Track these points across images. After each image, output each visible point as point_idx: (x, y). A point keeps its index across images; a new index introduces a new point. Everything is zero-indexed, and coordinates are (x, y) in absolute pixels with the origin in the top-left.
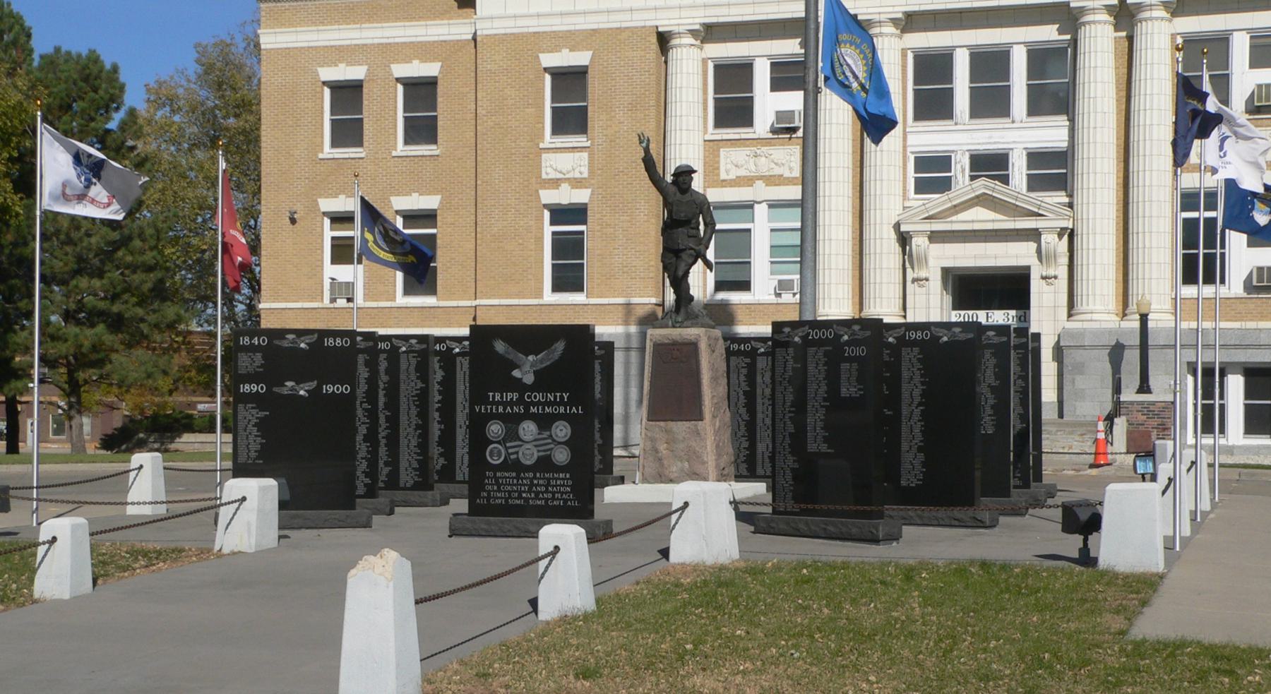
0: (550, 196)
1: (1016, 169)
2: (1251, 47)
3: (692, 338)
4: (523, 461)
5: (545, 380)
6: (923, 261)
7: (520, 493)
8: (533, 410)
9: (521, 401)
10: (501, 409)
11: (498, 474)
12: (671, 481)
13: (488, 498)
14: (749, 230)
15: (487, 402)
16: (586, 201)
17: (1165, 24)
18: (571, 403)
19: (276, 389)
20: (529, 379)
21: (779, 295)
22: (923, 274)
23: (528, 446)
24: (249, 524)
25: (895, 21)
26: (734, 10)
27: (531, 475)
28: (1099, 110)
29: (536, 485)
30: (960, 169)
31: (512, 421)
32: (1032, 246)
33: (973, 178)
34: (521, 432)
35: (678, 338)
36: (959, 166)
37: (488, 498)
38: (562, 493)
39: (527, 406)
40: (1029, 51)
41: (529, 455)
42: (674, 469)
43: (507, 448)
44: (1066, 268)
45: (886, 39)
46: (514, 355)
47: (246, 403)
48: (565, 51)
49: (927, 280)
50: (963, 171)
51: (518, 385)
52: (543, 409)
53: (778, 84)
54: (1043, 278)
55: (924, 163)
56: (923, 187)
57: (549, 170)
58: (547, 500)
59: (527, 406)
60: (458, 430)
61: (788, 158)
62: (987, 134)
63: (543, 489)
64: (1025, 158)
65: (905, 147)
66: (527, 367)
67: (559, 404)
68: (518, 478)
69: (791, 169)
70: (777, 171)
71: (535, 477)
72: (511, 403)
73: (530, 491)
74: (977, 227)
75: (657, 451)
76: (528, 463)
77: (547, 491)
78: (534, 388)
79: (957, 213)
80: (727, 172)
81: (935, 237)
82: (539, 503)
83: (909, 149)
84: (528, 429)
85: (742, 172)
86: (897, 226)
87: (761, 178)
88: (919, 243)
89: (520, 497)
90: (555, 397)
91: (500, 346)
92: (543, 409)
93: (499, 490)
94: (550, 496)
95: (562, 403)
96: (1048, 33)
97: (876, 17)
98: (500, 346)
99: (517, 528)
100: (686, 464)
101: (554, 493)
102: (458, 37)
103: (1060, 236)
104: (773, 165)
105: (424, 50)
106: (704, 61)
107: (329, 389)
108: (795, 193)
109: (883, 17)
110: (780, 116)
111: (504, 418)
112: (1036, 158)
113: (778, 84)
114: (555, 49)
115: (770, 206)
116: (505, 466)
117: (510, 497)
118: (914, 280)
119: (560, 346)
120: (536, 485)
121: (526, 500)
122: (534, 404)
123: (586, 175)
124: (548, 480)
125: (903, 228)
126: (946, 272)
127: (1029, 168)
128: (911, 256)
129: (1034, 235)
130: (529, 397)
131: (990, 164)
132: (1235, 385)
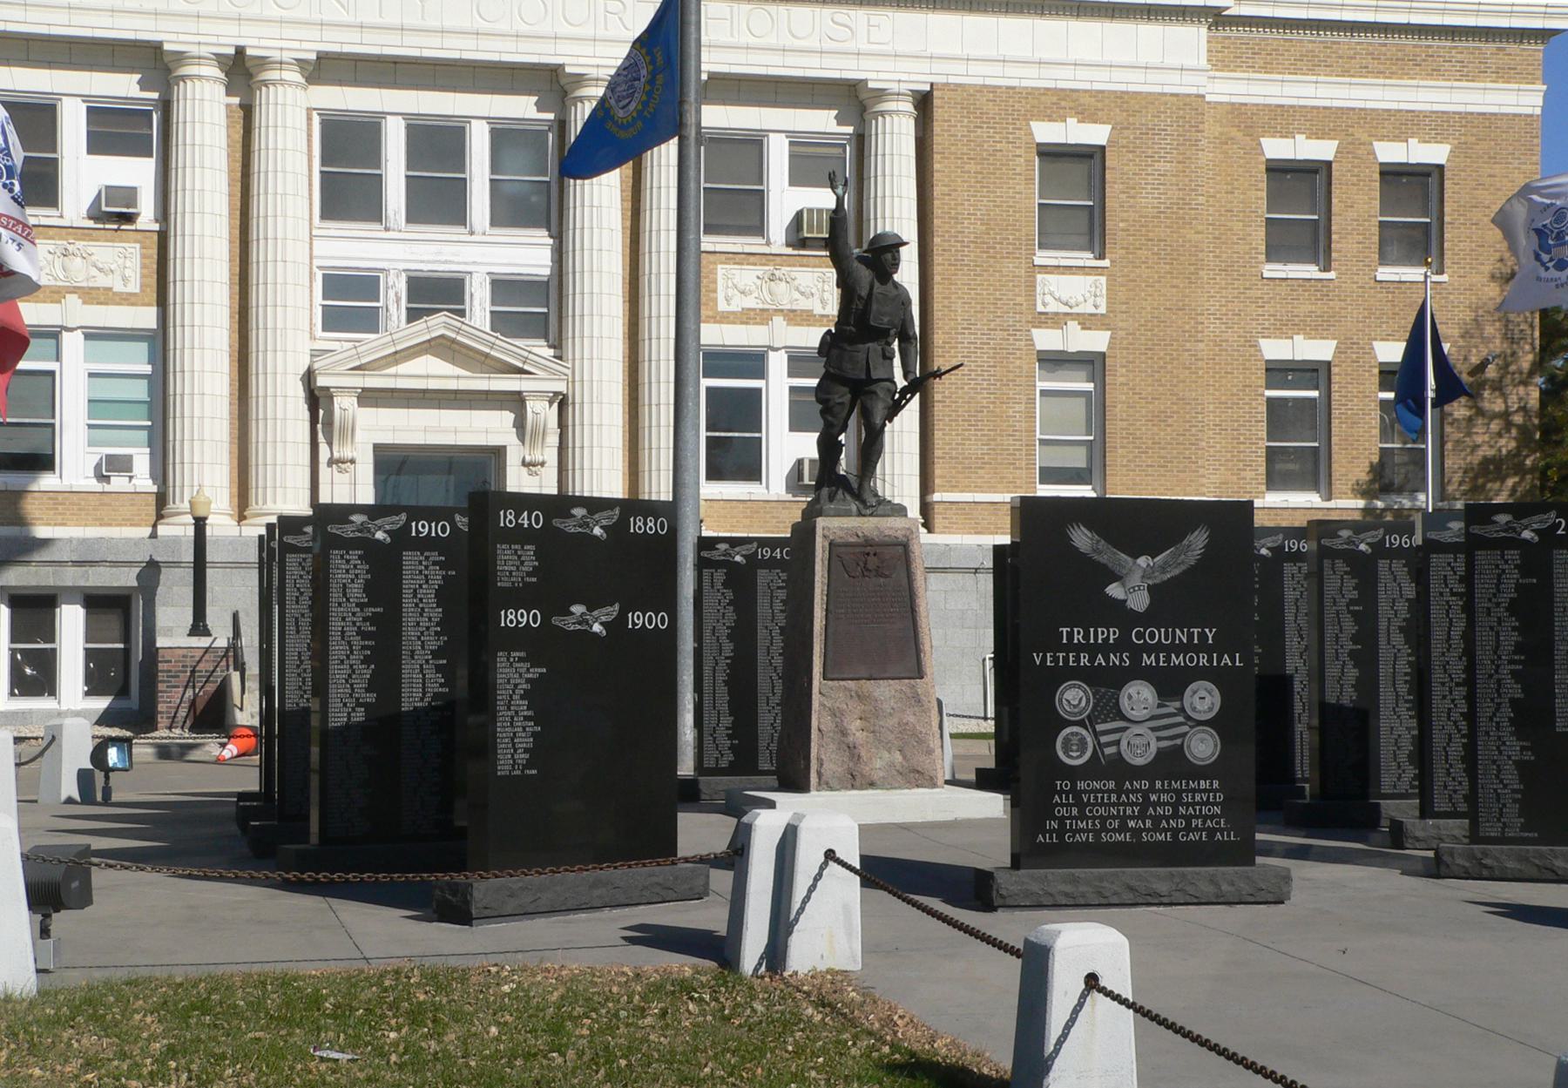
0: (1047, 340)
1: (476, 302)
2: (791, 156)
3: (899, 534)
4: (1128, 756)
5: (1170, 602)
6: (349, 432)
7: (1123, 820)
8: (1147, 660)
9: (1123, 644)
10: (1084, 660)
11: (1081, 785)
12: (872, 785)
13: (1061, 831)
14: (52, 373)
15: (1057, 646)
16: (1103, 348)
17: (299, 92)
18: (1220, 647)
19: (556, 621)
20: (1139, 601)
21: (106, 479)
22: (347, 453)
23: (1137, 729)
24: (846, 908)
25: (301, 63)
26: (78, 19)
27: (1145, 784)
28: (605, 225)
29: (1155, 805)
30: (394, 298)
31: (1106, 683)
32: (508, 417)
33: (413, 315)
34: (1125, 703)
35: (875, 535)
36: (391, 294)
37: (1061, 831)
38: (1205, 818)
39: (1136, 653)
40: (408, 127)
41: (1140, 747)
42: (879, 762)
43: (1096, 734)
44: (555, 451)
45: (289, 90)
46: (1110, 556)
47: (509, 649)
48: (1072, 121)
49: (352, 461)
50: (398, 301)
51: (1118, 613)
52: (1168, 659)
53: (99, 143)
54: (524, 464)
55: (337, 284)
56: (334, 320)
57: (1048, 298)
58: (1175, 832)
59: (1136, 653)
60: (762, 707)
61: (121, 262)
62: (434, 248)
63: (1169, 811)
64: (488, 287)
65: (311, 258)
66: (1135, 580)
67: (1197, 649)
68: (1119, 791)
69: (125, 279)
70: (102, 281)
71: (1152, 789)
72: (1105, 648)
73: (1142, 816)
74: (433, 385)
75: (844, 733)
76: (1139, 761)
77: (1175, 815)
78: (1146, 619)
79: (397, 363)
80: (1044, 304)
81: (369, 397)
82: (1161, 837)
83: (316, 262)
84: (1139, 697)
85: (751, 303)
86: (309, 377)
87: (74, 290)
88: (344, 405)
89: (1123, 828)
90: (1191, 636)
91: (1082, 538)
92: (1168, 659)
93: (1082, 817)
94: (1182, 823)
95: (1203, 647)
96: (123, 86)
97: (276, 55)
98: (1082, 538)
99: (1131, 889)
100: (898, 757)
101: (1188, 819)
102: (1327, 103)
103: (551, 403)
104: (94, 272)
105: (1319, 121)
106: (309, 110)
107: (637, 619)
108: (146, 317)
109: (287, 56)
110: (113, 193)
111: (1091, 677)
112: (503, 287)
113: (99, 143)
114: (1400, 136)
115: (88, 337)
116: (1094, 769)
117: (1104, 829)
118: (331, 462)
119: (1198, 540)
120: (1155, 805)
121: (1136, 832)
122: (1150, 650)
123: (1103, 310)
124: (1179, 792)
125: (321, 381)
126: (377, 448)
127: (493, 303)
128: (329, 424)
129: (515, 402)
130: (1140, 636)
131: (435, 293)
132: (71, 621)
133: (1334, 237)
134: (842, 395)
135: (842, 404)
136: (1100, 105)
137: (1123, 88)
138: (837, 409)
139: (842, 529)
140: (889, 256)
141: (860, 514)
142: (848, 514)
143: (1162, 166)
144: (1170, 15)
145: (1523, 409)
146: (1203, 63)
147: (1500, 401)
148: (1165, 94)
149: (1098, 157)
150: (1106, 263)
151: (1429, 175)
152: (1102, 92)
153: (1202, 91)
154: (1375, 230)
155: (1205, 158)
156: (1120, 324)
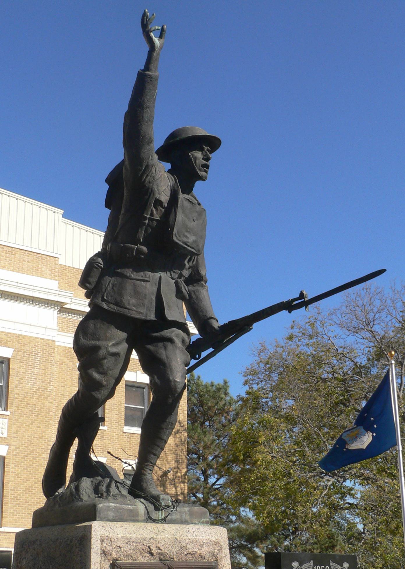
3: (205, 551)
35: (172, 551)
123: (5, 435)
133: (106, 411)
134: (115, 340)
135: (116, 355)
136: (9, 339)
137: (20, 333)
138: (108, 363)
139: (128, 541)
140: (199, 155)
141: (150, 519)
142: (131, 517)
143: (35, 370)
144: (39, 303)
145: (182, 493)
146: (55, 326)
147: (174, 489)
148: (38, 338)
149: (6, 363)
150: (8, 413)
151: (144, 388)
152: (10, 333)
153: (54, 339)
154: (123, 410)
155: (54, 369)
156: (13, 443)
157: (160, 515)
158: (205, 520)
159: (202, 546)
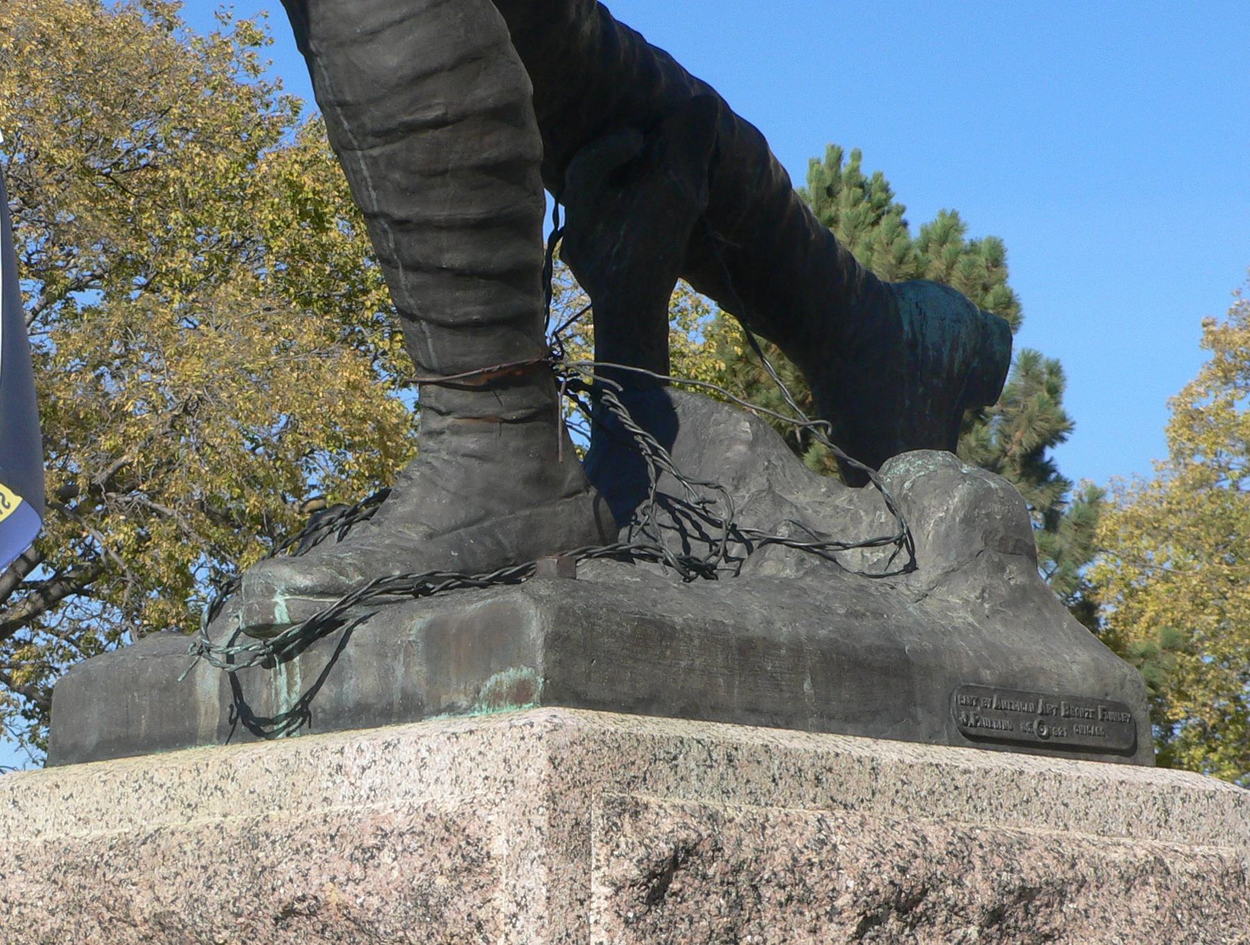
139: (68, 865)
141: (247, 723)
157: (281, 688)
158: (509, 676)
159: (367, 855)
